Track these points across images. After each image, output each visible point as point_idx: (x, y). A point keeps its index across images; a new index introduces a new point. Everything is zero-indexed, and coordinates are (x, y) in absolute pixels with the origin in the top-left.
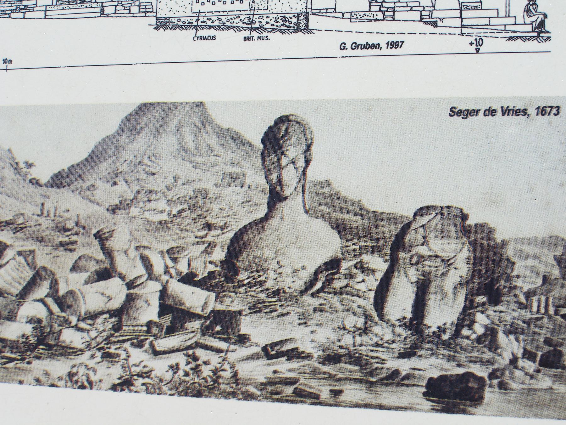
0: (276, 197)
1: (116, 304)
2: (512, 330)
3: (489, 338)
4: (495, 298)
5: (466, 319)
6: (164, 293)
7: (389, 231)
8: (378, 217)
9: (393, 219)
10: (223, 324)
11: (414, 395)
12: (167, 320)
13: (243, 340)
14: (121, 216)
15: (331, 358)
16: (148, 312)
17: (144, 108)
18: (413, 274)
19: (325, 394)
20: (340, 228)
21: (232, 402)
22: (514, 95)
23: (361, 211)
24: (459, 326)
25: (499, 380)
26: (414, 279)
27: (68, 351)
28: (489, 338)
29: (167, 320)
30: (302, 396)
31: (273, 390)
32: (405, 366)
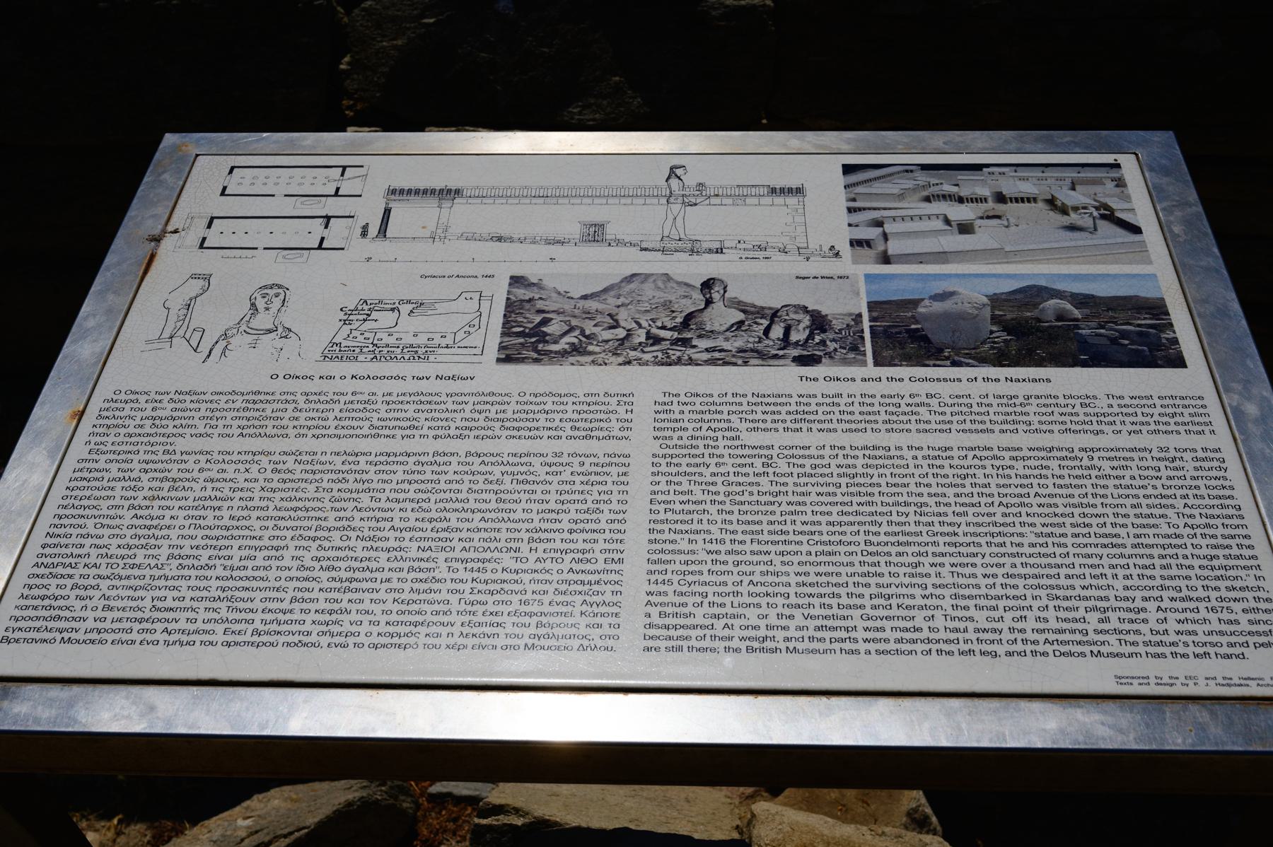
0: (709, 302)
1: (621, 336)
2: (833, 340)
3: (823, 342)
4: (824, 331)
5: (811, 336)
6: (648, 333)
7: (769, 312)
8: (763, 308)
9: (770, 308)
10: (686, 342)
11: (788, 361)
12: (651, 341)
13: (694, 347)
14: (622, 309)
15: (741, 351)
16: (640, 337)
17: (634, 275)
18: (782, 325)
19: (740, 362)
20: (744, 311)
21: (689, 367)
22: (826, 272)
23: (755, 306)
24: (807, 340)
25: (377, 792)
26: (834, 322)
27: (590, 353)
28: (823, 342)
29: (651, 341)
30: (726, 363)
31: (712, 362)
32: (781, 353)
